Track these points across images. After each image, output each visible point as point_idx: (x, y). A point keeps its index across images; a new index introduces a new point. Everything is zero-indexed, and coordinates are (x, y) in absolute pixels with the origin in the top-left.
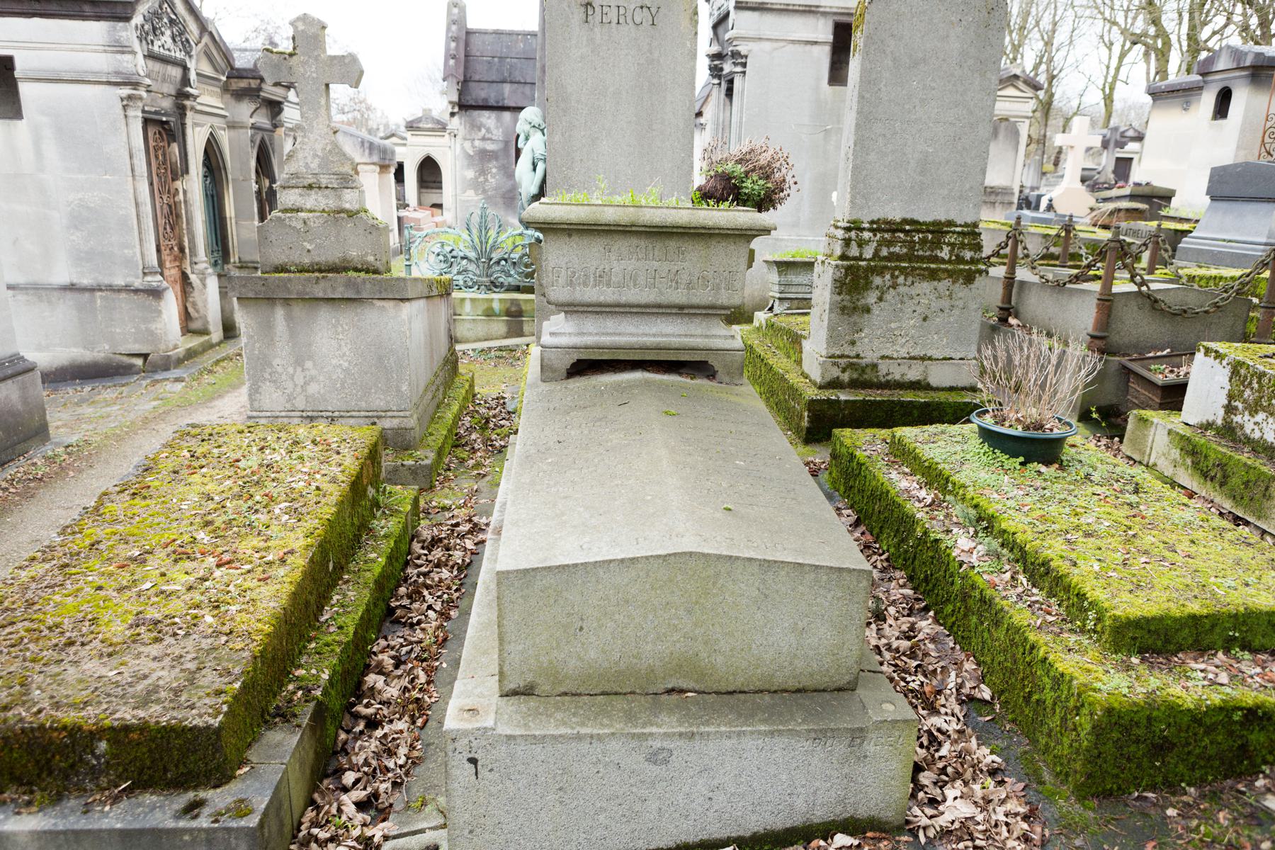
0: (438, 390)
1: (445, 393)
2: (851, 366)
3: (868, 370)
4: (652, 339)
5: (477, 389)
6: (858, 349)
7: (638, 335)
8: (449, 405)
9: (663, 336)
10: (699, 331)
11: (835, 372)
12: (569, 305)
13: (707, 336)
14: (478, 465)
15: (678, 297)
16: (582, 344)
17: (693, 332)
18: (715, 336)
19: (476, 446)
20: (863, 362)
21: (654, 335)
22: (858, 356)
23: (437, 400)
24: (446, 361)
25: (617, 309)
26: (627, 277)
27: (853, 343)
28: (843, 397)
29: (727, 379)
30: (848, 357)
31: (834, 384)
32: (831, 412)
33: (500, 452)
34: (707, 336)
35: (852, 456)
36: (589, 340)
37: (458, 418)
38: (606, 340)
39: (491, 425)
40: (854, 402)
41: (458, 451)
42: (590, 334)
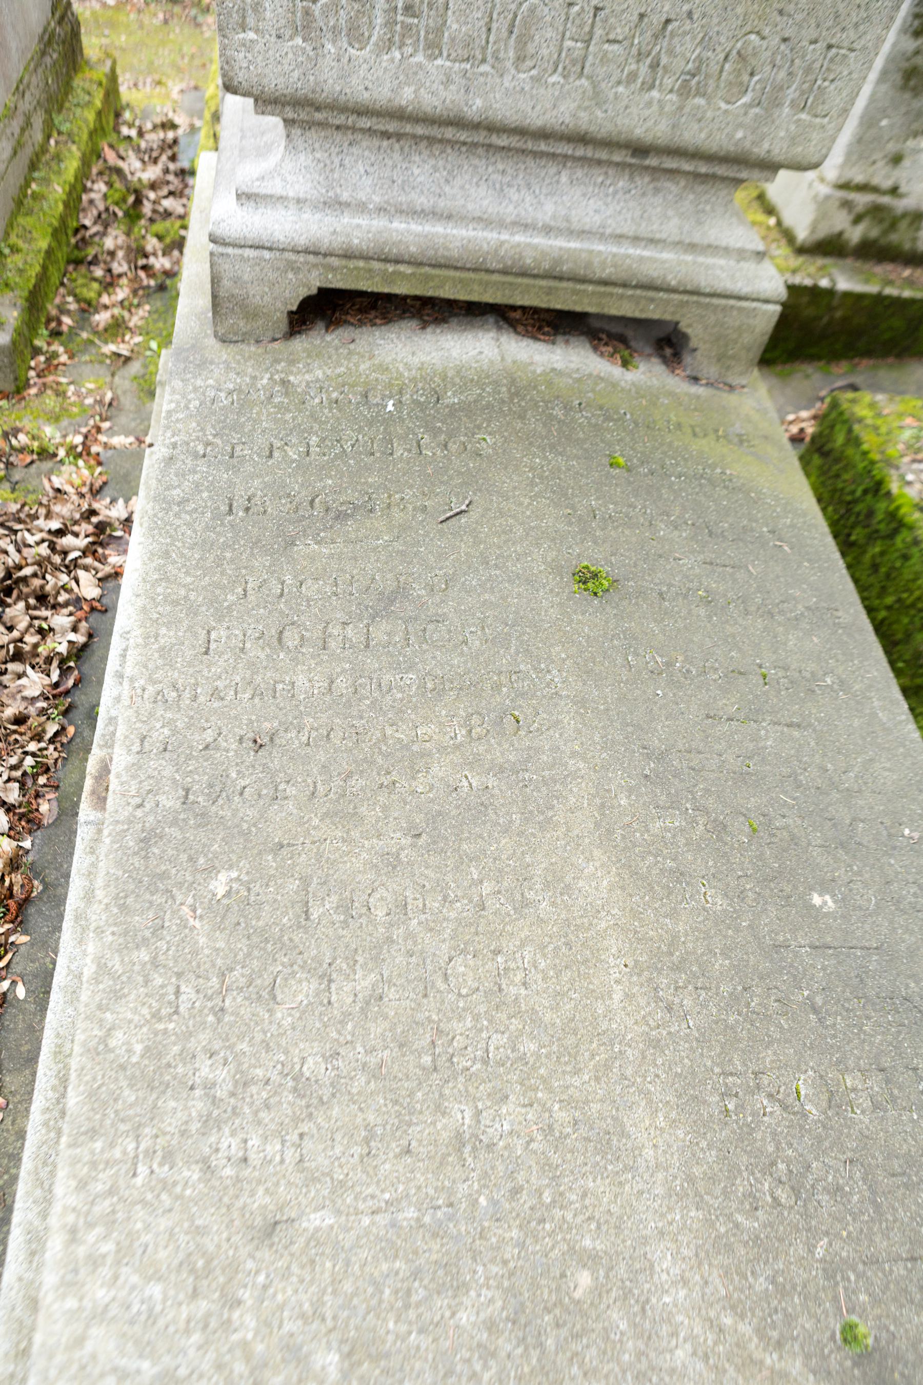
0: (27, 124)
1: (49, 128)
2: (876, 212)
3: (903, 225)
4: (539, 240)
5: (126, 93)
6: (901, 175)
7: (501, 224)
8: (58, 158)
9: (572, 233)
10: (671, 228)
11: (840, 222)
12: (298, 102)
13: (692, 247)
14: (117, 328)
15: (645, 114)
16: (338, 243)
17: (655, 228)
18: (712, 249)
19: (117, 268)
20: (901, 205)
21: (548, 230)
22: (894, 191)
23: (27, 152)
24: (47, 41)
25: (449, 133)
26: (500, 25)
27: (897, 160)
28: (844, 284)
29: (711, 371)
30: (875, 190)
31: (828, 247)
32: (810, 312)
33: (162, 288)
34: (692, 247)
35: (877, 488)
36: (359, 229)
37: (77, 190)
38: (408, 233)
39: (147, 208)
40: (860, 297)
41: (78, 277)
42: (361, 207)
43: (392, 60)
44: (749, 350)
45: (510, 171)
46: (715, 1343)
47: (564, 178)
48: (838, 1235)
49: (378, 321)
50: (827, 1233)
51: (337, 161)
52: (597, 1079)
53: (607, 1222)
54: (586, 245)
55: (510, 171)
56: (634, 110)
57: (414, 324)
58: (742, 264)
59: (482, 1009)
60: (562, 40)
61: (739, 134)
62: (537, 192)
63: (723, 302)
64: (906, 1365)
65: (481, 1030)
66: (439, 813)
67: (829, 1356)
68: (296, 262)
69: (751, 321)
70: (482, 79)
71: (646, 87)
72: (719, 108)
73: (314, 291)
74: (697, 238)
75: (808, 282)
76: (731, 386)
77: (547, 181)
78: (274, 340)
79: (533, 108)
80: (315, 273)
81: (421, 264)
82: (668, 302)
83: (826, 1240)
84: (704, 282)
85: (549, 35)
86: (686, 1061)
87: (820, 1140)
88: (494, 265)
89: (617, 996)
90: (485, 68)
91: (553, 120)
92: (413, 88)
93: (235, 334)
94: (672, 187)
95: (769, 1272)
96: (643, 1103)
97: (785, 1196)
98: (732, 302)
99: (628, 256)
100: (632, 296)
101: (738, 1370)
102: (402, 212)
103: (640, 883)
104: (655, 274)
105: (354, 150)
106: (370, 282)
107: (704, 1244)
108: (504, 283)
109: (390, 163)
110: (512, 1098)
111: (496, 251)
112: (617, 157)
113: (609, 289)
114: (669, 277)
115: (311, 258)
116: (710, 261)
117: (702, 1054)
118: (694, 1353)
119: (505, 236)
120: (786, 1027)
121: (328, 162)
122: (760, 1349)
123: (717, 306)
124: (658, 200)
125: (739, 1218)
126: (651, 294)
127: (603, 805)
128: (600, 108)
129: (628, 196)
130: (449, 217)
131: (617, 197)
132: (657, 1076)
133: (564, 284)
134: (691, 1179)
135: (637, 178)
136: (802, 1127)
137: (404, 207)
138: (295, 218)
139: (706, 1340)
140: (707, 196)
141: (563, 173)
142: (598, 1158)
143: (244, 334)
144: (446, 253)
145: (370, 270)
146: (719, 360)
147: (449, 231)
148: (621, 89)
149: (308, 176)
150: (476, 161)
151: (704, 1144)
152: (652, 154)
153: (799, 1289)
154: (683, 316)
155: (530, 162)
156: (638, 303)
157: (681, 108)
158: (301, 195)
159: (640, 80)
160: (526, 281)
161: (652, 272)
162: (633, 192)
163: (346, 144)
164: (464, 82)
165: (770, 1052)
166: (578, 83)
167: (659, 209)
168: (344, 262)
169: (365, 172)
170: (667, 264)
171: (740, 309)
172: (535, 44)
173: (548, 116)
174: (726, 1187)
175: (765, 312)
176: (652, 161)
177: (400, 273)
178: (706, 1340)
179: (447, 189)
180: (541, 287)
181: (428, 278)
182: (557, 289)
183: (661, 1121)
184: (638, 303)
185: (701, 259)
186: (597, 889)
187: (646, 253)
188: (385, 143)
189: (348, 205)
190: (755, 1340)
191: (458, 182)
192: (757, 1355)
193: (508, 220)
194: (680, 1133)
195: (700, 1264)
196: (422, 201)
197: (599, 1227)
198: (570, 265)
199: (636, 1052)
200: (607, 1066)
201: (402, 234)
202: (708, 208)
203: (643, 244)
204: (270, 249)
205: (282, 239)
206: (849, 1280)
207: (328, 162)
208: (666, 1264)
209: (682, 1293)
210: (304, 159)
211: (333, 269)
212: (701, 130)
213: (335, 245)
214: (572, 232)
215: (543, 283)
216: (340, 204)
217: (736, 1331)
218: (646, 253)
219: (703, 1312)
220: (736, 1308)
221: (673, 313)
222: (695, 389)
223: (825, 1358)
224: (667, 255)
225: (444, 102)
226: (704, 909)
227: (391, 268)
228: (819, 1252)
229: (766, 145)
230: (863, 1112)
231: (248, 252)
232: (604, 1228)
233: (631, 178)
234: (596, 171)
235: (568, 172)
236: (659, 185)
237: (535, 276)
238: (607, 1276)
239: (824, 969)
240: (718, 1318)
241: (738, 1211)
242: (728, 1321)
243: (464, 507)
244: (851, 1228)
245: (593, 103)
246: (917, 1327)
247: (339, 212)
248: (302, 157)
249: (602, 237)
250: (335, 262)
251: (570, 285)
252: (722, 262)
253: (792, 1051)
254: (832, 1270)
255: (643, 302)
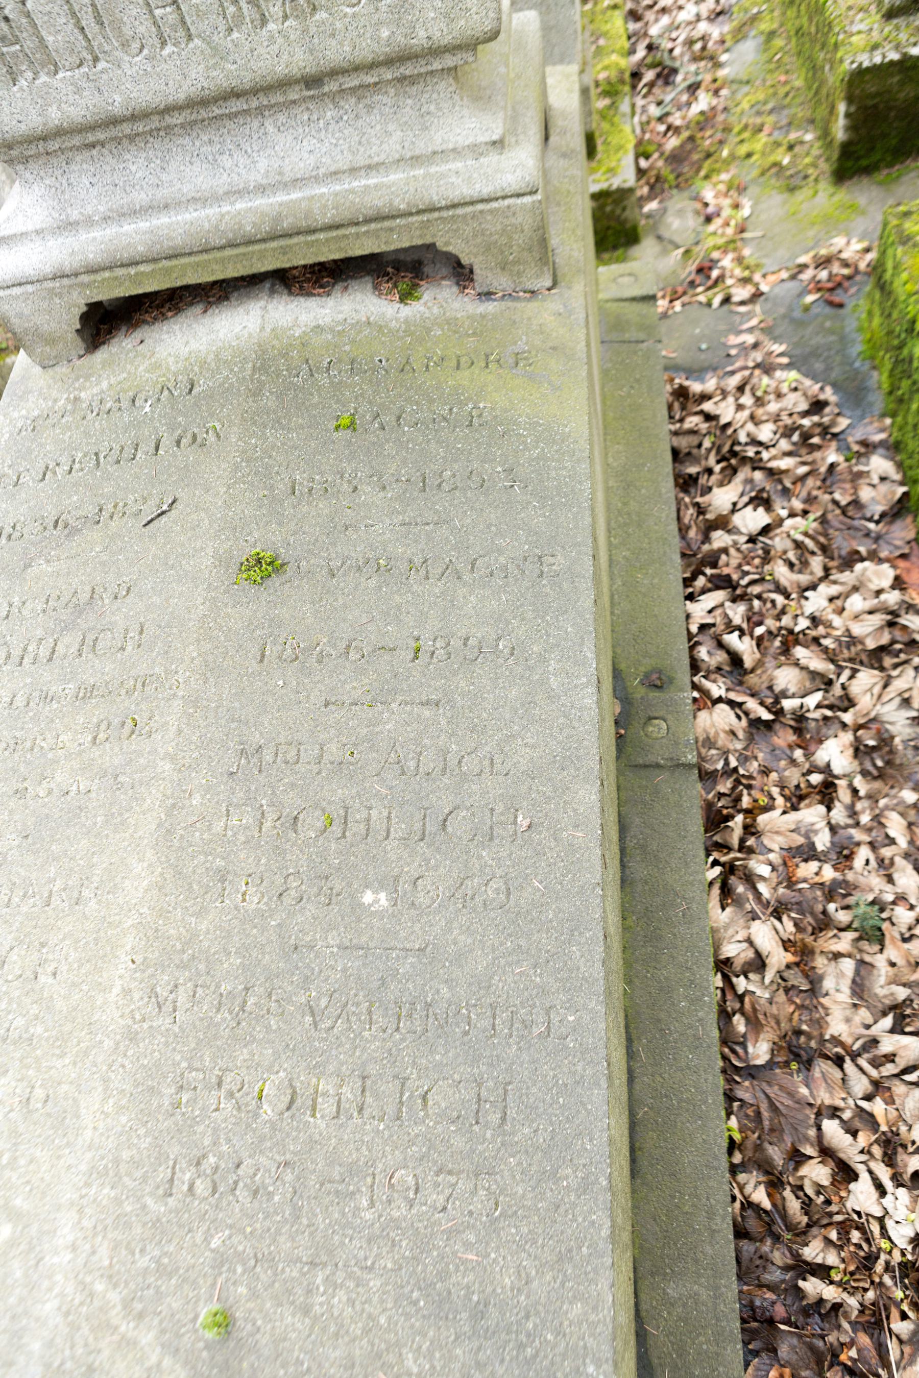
4: (260, 202)
7: (214, 198)
13: (416, 160)
21: (261, 189)
29: (501, 282)
42: (89, 222)
43: (21, 89)
44: (530, 250)
45: (216, 139)
46: (82, 1304)
47: (271, 129)
48: (242, 1231)
49: (170, 314)
50: (231, 1227)
51: (64, 182)
52: (75, 1064)
53: (38, 1187)
54: (308, 192)
55: (216, 139)
56: (261, 50)
57: (198, 309)
58: (482, 160)
59: (17, 993)
60: (151, 12)
61: (385, 33)
62: (249, 150)
63: (469, 209)
64: (258, 1358)
65: (9, 1012)
66: (47, 815)
67: (183, 1335)
68: (54, 288)
69: (513, 220)
70: (105, 76)
71: (258, 23)
72: (345, 15)
73: (85, 309)
74: (421, 147)
75: (894, 56)
76: (533, 292)
77: (255, 137)
78: (81, 357)
79: (167, 84)
80: (75, 294)
81: (155, 260)
82: (408, 227)
83: (227, 1232)
84: (436, 194)
85: (134, 13)
86: (156, 1054)
87: (262, 1139)
88: (218, 242)
89: (116, 990)
90: (101, 65)
91: (193, 89)
92: (55, 107)
93: (49, 359)
94: (385, 99)
95: (157, 1253)
96: (100, 1089)
97: (202, 1187)
98: (480, 207)
99: (352, 191)
100: (368, 232)
101: (92, 1330)
102: (124, 215)
103: (180, 883)
104: (380, 204)
105: (73, 167)
106: (123, 288)
107: (105, 1219)
108: (237, 255)
109: (108, 168)
110: (10, 1073)
111: (217, 227)
112: (293, 95)
113: (341, 232)
114: (396, 202)
115: (66, 281)
116: (444, 168)
117: (174, 1049)
118: (59, 1308)
119: (226, 208)
120: (274, 1027)
121: (58, 185)
122: (121, 1316)
123: (464, 216)
124: (375, 117)
125: (149, 1201)
126: (387, 224)
127: (174, 806)
128: (227, 61)
129: (341, 124)
130: (166, 206)
131: (331, 128)
132: (123, 1066)
133: (295, 240)
134: (117, 1161)
135: (342, 103)
136: (248, 1126)
137: (125, 210)
138: (41, 249)
139: (73, 1299)
140: (426, 96)
141: (266, 124)
142: (51, 1132)
143: (56, 357)
144: (170, 244)
145: (116, 278)
146: (503, 269)
147: (174, 219)
148: (235, 35)
149: (44, 204)
150: (181, 141)
151: (142, 1131)
152: (326, 79)
153: (181, 1271)
154: (434, 236)
155: (230, 124)
156: (378, 237)
157: (305, 31)
158: (38, 227)
159: (248, 19)
160: (257, 247)
161: (378, 202)
162: (345, 118)
163: (64, 164)
164: (91, 84)
165: (245, 1051)
166: (191, 45)
167: (378, 127)
168: (92, 277)
169: (91, 186)
170: (395, 187)
171: (491, 211)
172: (129, 26)
173: (185, 87)
174: (147, 1172)
175: (523, 207)
176: (331, 86)
177: (142, 273)
178: (73, 1299)
179: (164, 177)
180: (274, 250)
181: (168, 271)
182: (290, 247)
183: (109, 1107)
184: (378, 237)
185: (433, 169)
186: (136, 889)
187: (372, 181)
188: (95, 152)
189: (77, 223)
190: (119, 1307)
191: (173, 166)
192: (115, 1321)
193: (221, 192)
194: (124, 1119)
195: (95, 1235)
196: (140, 197)
197: (31, 1190)
198: (290, 220)
199: (112, 1043)
200: (86, 1053)
201: (131, 236)
202: (432, 108)
203: (363, 172)
204: (32, 283)
205: (32, 272)
206: (235, 1271)
207: (58, 185)
208: (66, 1233)
209: (69, 1256)
210: (38, 189)
211: (88, 286)
212: (341, 44)
213: (75, 265)
214: (285, 185)
215: (274, 244)
216: (71, 224)
217: (104, 1297)
218: (372, 181)
219: (80, 1276)
220: (112, 1280)
221: (421, 236)
222: (490, 307)
223: (178, 1336)
224: (395, 177)
225: (88, 108)
226: (236, 908)
227: (132, 271)
228: (215, 1243)
229: (422, 34)
230: (322, 1117)
231: (16, 291)
232: (34, 1192)
233: (336, 106)
234: (297, 110)
235: (271, 120)
236: (368, 101)
237: (263, 240)
238: (22, 1232)
239: (344, 970)
240: (92, 1283)
241: (151, 1194)
242: (99, 1287)
243: (165, 507)
244: (258, 1226)
245: (217, 59)
246: (286, 1326)
247: (74, 232)
248: (35, 186)
249: (317, 179)
250: (85, 278)
251: (301, 238)
252: (459, 165)
253: (270, 1051)
254: (220, 1261)
255: (383, 234)
